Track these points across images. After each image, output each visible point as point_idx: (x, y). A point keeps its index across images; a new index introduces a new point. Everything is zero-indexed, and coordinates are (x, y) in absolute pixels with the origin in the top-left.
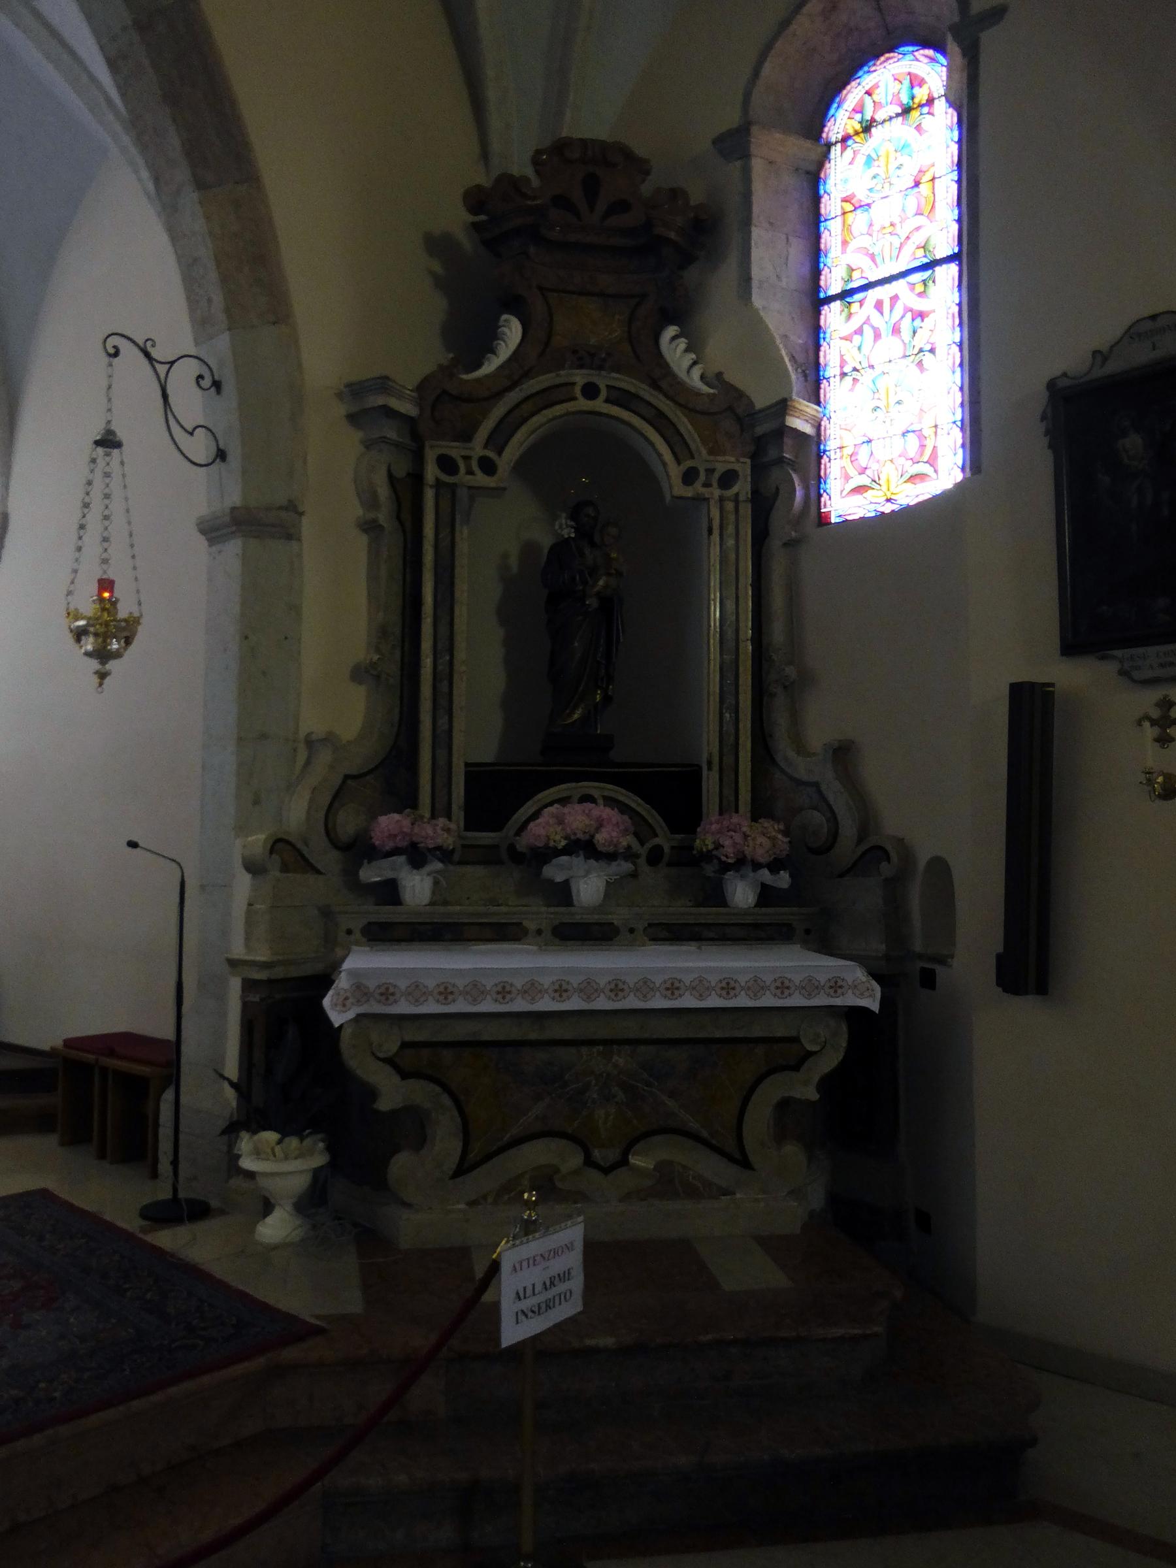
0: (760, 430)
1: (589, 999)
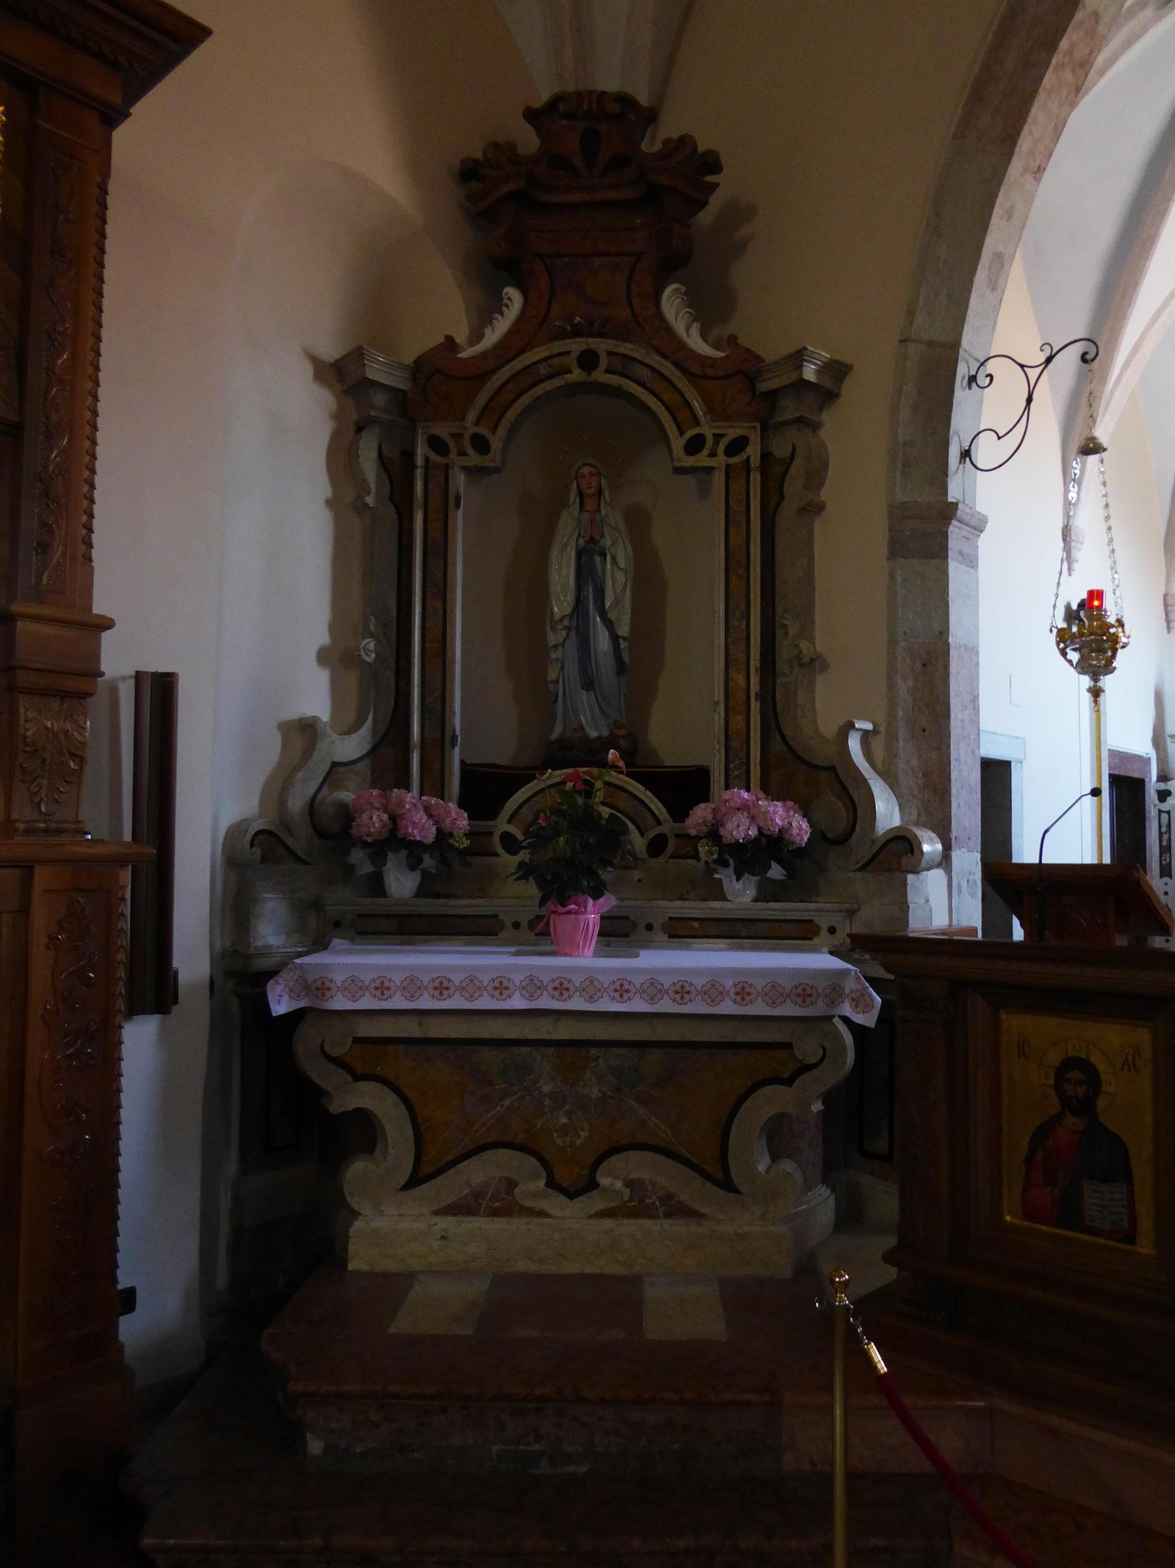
0: (763, 387)
1: (652, 1000)
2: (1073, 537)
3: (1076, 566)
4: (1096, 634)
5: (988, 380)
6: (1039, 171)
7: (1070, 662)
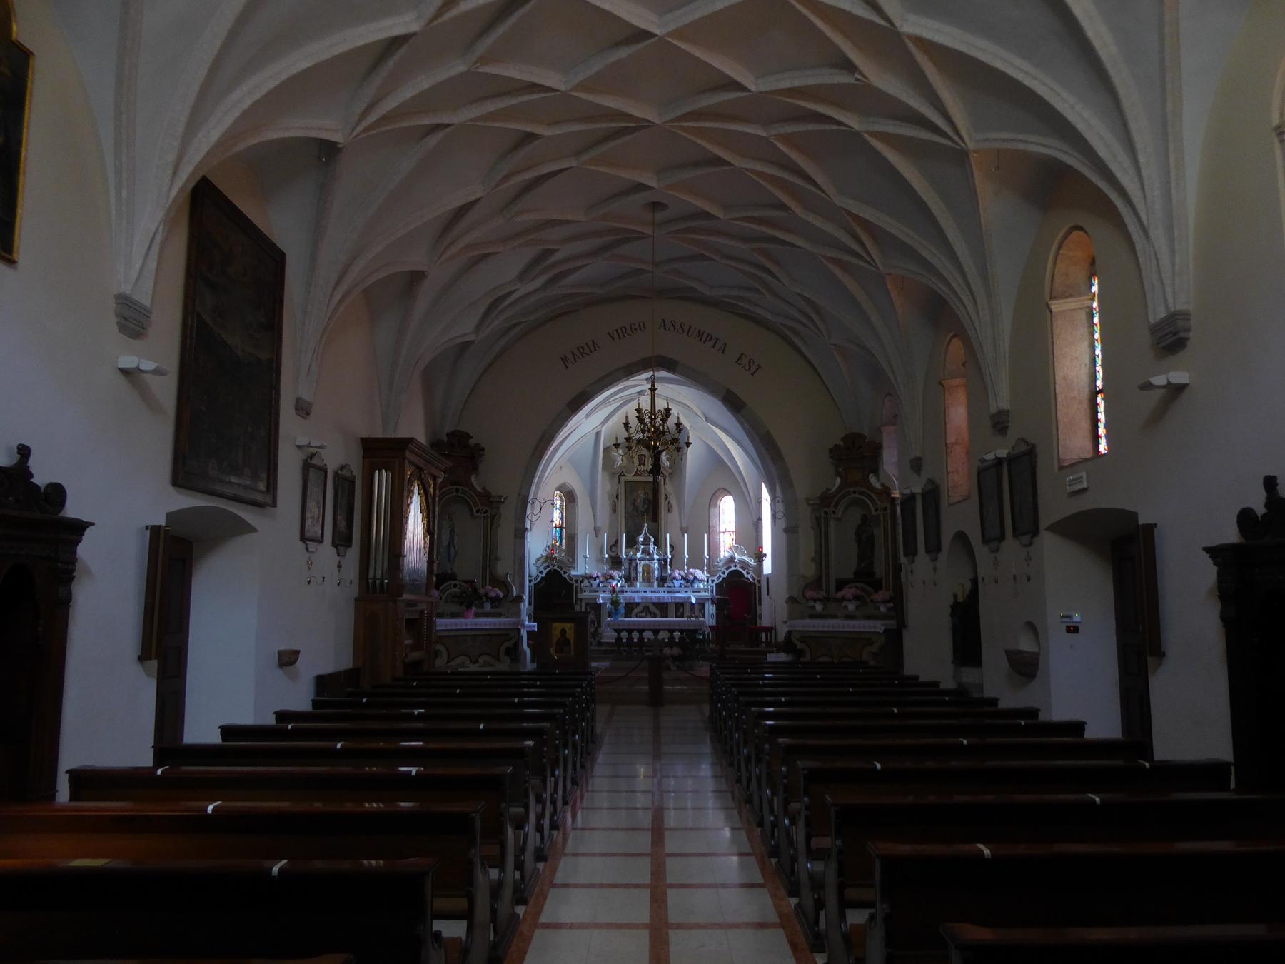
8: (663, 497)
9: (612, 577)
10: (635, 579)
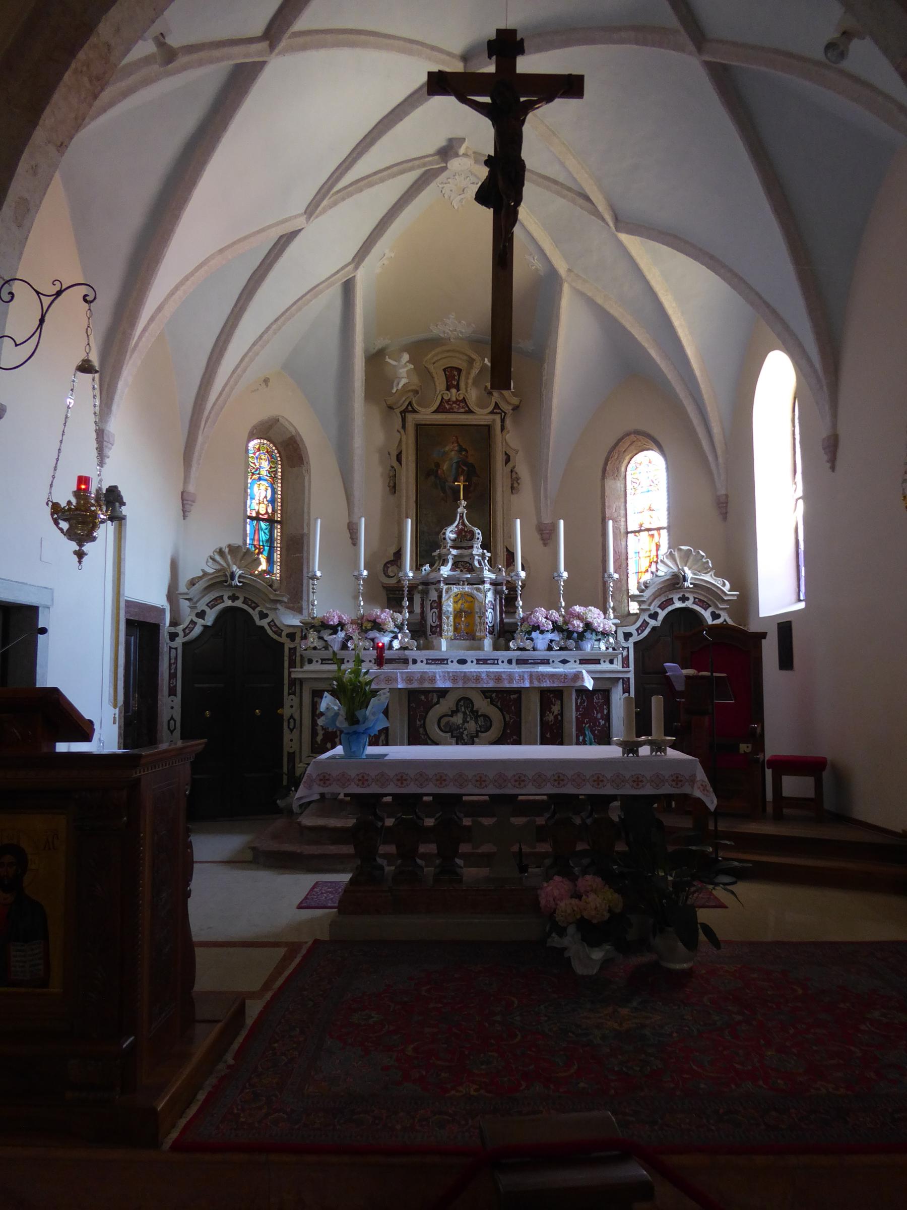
2: (106, 439)
3: (107, 460)
4: (80, 510)
5: (9, 297)
6: (62, 147)
7: (61, 530)
8: (499, 458)
9: (377, 626)
10: (438, 630)
